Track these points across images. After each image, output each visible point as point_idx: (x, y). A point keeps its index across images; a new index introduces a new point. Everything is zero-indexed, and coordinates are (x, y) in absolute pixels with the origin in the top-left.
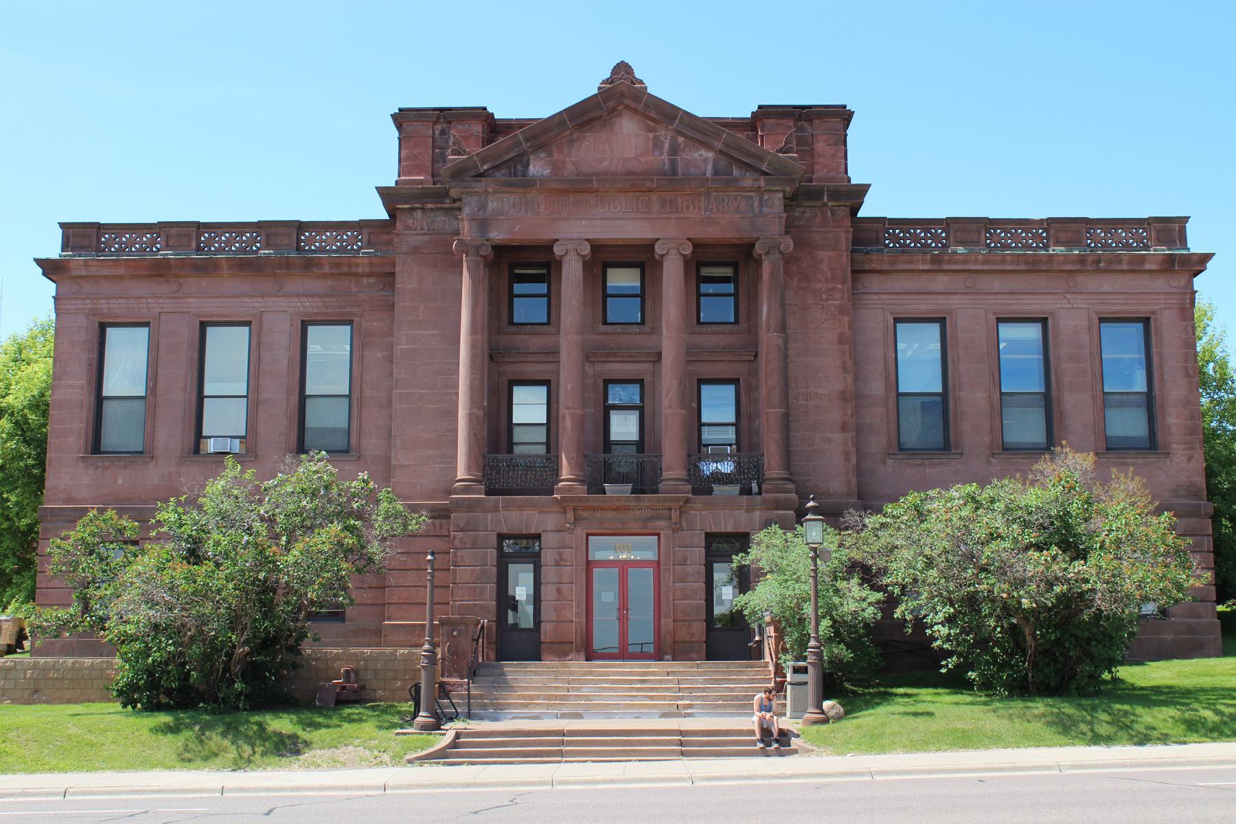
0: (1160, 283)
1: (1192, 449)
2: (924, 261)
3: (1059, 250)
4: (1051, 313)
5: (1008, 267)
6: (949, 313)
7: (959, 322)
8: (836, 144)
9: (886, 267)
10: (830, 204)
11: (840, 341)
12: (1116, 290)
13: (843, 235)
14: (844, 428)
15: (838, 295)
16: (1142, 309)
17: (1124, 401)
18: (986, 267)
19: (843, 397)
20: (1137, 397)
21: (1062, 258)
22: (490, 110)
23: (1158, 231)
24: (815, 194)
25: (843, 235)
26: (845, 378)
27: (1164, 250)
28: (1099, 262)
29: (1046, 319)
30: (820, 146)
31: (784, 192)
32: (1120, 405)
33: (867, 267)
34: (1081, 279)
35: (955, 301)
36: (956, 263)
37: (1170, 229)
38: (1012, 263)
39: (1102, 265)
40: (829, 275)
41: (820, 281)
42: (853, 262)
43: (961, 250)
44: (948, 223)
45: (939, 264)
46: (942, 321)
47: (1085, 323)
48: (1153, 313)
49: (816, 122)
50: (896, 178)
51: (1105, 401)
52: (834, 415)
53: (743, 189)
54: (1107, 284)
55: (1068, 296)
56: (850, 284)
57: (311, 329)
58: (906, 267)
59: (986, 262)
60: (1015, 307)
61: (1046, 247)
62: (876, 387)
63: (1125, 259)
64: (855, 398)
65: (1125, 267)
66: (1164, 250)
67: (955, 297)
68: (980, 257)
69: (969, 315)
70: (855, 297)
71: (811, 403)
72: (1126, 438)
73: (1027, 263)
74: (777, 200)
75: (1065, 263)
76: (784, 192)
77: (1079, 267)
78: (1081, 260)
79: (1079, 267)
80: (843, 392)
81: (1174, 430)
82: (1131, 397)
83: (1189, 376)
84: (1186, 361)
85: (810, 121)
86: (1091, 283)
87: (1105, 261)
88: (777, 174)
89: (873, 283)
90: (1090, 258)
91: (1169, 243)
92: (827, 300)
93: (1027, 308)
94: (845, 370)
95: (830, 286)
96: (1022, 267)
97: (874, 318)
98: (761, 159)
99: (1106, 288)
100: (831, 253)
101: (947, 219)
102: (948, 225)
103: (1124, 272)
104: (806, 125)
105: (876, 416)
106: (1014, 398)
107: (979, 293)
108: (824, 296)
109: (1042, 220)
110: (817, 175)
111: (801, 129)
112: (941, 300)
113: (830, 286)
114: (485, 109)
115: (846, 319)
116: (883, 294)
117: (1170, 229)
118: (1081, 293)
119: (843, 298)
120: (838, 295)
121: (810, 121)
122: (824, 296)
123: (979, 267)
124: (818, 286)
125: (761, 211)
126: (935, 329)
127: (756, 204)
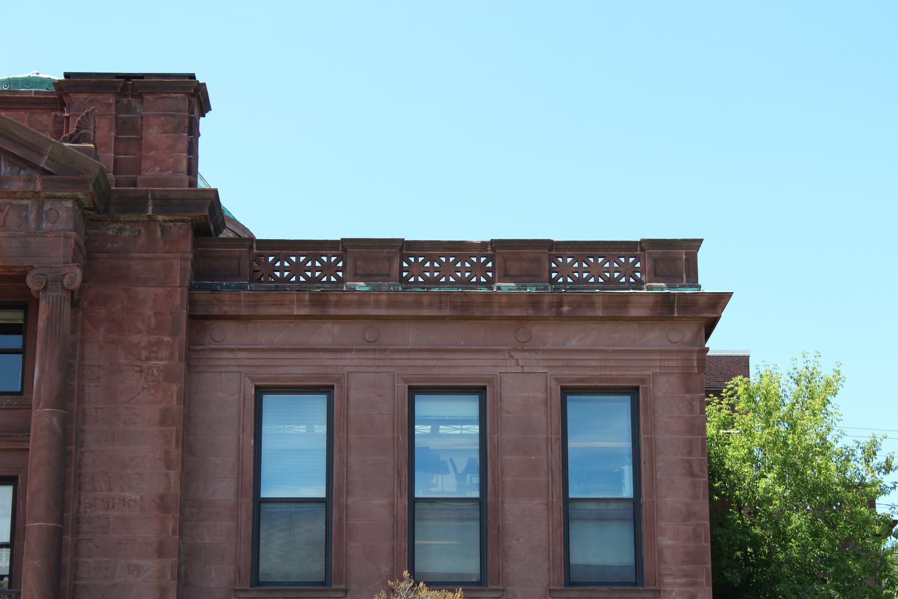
0: (655, 337)
1: (694, 584)
2: (301, 304)
3: (507, 286)
4: (490, 381)
5: (425, 312)
6: (338, 380)
7: (352, 393)
8: (176, 130)
9: (244, 311)
10: (160, 218)
11: (163, 422)
12: (585, 345)
13: (177, 264)
14: (161, 551)
15: (164, 353)
16: (629, 374)
17: (602, 511)
18: (393, 312)
19: (163, 504)
20: (621, 505)
21: (504, 300)
22: (200, 79)
23: (656, 260)
24: (135, 204)
25: (177, 264)
26: (167, 475)
27: (661, 287)
28: (560, 305)
29: (484, 388)
30: (153, 133)
31: (77, 200)
32: (601, 518)
33: (216, 311)
34: (537, 329)
35: (348, 361)
36: (348, 305)
37: (675, 258)
38: (431, 306)
39: (565, 309)
40: (153, 321)
41: (139, 332)
42: (192, 303)
43: (361, 286)
44: (346, 248)
45: (322, 304)
46: (633, 391)
47: (541, 396)
48: (643, 380)
49: (149, 97)
50: (265, 177)
51: (567, 511)
52: (147, 531)
53: (12, 195)
54: (575, 337)
55: (517, 355)
56: (183, 336)
57: (267, 399)
58: (273, 311)
59: (392, 304)
60: (436, 371)
61: (490, 282)
62: (223, 489)
63: (599, 300)
64: (184, 507)
65: (599, 313)
66: (661, 287)
67: (348, 355)
68: (383, 297)
69: (370, 382)
70: (193, 356)
71: (114, 513)
72: (604, 568)
73: (454, 306)
74: (64, 213)
75: (511, 306)
76: (77, 200)
77: (531, 312)
78: (534, 302)
79: (531, 312)
80: (162, 497)
81: (668, 555)
82: (612, 506)
83: (692, 474)
84: (690, 453)
85: (140, 96)
86: (552, 336)
87: (570, 304)
88: (63, 174)
89: (228, 334)
90: (547, 299)
91: (671, 277)
92: (148, 359)
93: (453, 372)
94: (168, 463)
95: (153, 338)
96: (447, 312)
97: (225, 388)
98: (39, 152)
99: (573, 343)
100: (160, 291)
101: (493, 242)
102: (345, 250)
103: (602, 319)
104: (135, 102)
105: (220, 533)
106: (436, 506)
107: (385, 350)
108: (144, 354)
109: (483, 243)
110: (146, 175)
111: (129, 109)
112: (327, 359)
113: (153, 338)
114: (192, 77)
115: (175, 388)
116: (238, 354)
117: (675, 258)
118: (536, 351)
119: (171, 357)
120: (164, 353)
121: (140, 96)
122: (144, 354)
123: (383, 312)
124: (136, 338)
125: (38, 227)
126: (624, 403)
127: (32, 216)
